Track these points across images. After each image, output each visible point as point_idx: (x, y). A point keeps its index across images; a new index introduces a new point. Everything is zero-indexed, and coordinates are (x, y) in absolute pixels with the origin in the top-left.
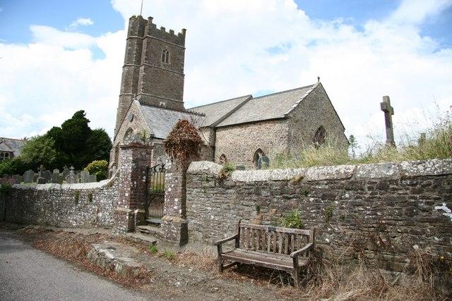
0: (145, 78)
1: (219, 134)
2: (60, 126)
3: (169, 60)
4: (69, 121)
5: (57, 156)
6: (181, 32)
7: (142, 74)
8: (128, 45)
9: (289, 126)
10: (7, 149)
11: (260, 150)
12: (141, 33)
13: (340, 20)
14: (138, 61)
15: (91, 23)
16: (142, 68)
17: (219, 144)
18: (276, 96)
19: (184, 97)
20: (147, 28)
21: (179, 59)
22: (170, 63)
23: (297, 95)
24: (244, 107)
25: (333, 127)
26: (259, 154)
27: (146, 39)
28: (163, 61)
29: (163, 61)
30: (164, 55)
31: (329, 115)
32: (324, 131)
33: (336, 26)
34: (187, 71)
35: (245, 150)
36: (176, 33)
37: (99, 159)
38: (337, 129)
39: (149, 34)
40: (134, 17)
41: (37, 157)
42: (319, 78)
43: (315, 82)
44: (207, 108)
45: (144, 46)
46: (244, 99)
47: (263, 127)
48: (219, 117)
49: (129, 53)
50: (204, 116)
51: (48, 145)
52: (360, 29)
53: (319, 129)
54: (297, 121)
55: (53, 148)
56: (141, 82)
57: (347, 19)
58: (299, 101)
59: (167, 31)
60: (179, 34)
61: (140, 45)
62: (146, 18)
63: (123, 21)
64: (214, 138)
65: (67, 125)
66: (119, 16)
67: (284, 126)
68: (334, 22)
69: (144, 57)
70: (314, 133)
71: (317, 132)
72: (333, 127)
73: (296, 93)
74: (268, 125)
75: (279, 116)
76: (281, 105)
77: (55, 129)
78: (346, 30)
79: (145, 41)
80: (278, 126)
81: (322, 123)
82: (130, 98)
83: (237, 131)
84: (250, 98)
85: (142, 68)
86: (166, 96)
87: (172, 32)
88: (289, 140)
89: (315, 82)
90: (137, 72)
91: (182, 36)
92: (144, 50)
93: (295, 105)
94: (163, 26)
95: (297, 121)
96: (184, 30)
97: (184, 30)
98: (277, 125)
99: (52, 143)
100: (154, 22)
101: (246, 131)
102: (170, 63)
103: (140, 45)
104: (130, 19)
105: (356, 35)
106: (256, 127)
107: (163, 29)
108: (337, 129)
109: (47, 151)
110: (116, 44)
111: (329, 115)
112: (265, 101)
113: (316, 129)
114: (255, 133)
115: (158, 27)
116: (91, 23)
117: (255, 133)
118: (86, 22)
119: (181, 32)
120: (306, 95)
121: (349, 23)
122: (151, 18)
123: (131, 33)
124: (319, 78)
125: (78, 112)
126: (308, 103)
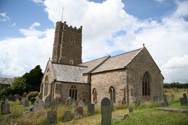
0: (63, 50)
1: (92, 77)
2: (29, 72)
3: (74, 41)
4: (33, 70)
5: (26, 86)
6: (80, 27)
7: (61, 48)
8: (56, 35)
9: (127, 73)
10: (7, 83)
11: (112, 87)
12: (61, 29)
13: (151, 19)
14: (60, 42)
15: (39, 25)
16: (61, 45)
17: (93, 82)
18: (121, 56)
19: (82, 58)
20: (64, 26)
21: (79, 40)
22: (75, 42)
23: (132, 55)
24: (106, 62)
25: (154, 71)
26: (112, 89)
27: (63, 32)
28: (71, 41)
29: (71, 41)
30: (72, 39)
31: (151, 65)
32: (149, 74)
33: (150, 21)
34: (83, 45)
35: (105, 86)
36: (78, 28)
37: (33, 91)
38: (156, 72)
39: (64, 29)
40: (58, 22)
41: (17, 87)
42: (144, 45)
43: (142, 47)
44: (87, 63)
45: (63, 35)
46: (106, 58)
47: (114, 73)
48: (93, 68)
49: (56, 38)
50: (87, 67)
51: (23, 81)
52: (160, 21)
53: (146, 73)
54: (132, 70)
55: (25, 83)
56: (61, 52)
57: (154, 18)
58: (132, 58)
59: (73, 27)
60: (79, 28)
61: (61, 34)
62: (63, 22)
63: (54, 24)
64: (90, 79)
65: (32, 71)
66: (52, 23)
67: (124, 74)
68: (148, 19)
69: (62, 40)
70: (142, 76)
71: (145, 75)
72: (154, 71)
73: (136, 51)
74: (116, 73)
75: (121, 67)
76: (123, 60)
77: (27, 74)
78: (154, 23)
79: (63, 33)
80: (121, 73)
81: (147, 69)
82: (56, 59)
83: (100, 75)
84: (110, 57)
85: (61, 45)
86: (73, 57)
87: (75, 28)
88: (128, 81)
89: (142, 47)
90: (59, 47)
91: (80, 30)
92: (62, 37)
93: (130, 61)
94: (71, 26)
95: (132, 70)
96: (81, 27)
97: (81, 27)
98: (121, 72)
99: (25, 81)
100: (67, 24)
101: (105, 75)
102: (75, 42)
103: (61, 34)
104: (56, 23)
105: (158, 24)
106: (110, 73)
107: (71, 27)
108: (156, 72)
109: (22, 84)
110: (51, 34)
111: (151, 65)
112: (116, 59)
113: (143, 73)
114: (109, 77)
115: (69, 26)
116: (39, 25)
117: (109, 77)
118: (38, 24)
119: (80, 27)
120: (137, 54)
121: (155, 20)
122: (65, 22)
123: (57, 29)
124: (144, 45)
125: (37, 66)
126: (138, 59)
